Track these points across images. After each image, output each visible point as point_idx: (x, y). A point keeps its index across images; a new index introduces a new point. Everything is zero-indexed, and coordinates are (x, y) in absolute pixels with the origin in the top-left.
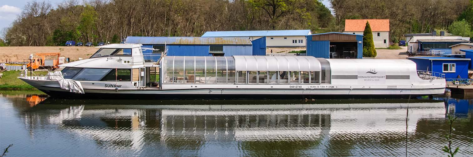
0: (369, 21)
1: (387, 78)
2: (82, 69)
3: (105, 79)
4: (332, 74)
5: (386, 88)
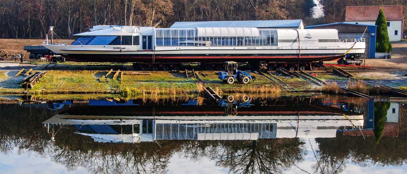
0: (382, 8)
1: (319, 42)
2: (95, 36)
3: (113, 43)
4: (279, 39)
5: (318, 49)
